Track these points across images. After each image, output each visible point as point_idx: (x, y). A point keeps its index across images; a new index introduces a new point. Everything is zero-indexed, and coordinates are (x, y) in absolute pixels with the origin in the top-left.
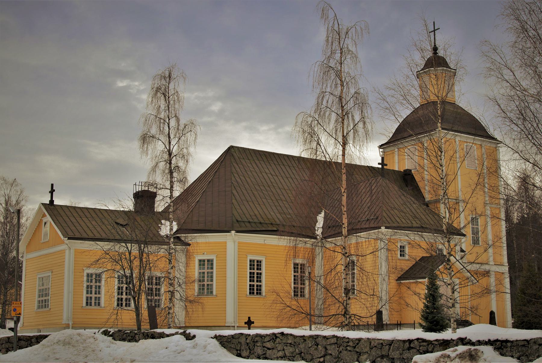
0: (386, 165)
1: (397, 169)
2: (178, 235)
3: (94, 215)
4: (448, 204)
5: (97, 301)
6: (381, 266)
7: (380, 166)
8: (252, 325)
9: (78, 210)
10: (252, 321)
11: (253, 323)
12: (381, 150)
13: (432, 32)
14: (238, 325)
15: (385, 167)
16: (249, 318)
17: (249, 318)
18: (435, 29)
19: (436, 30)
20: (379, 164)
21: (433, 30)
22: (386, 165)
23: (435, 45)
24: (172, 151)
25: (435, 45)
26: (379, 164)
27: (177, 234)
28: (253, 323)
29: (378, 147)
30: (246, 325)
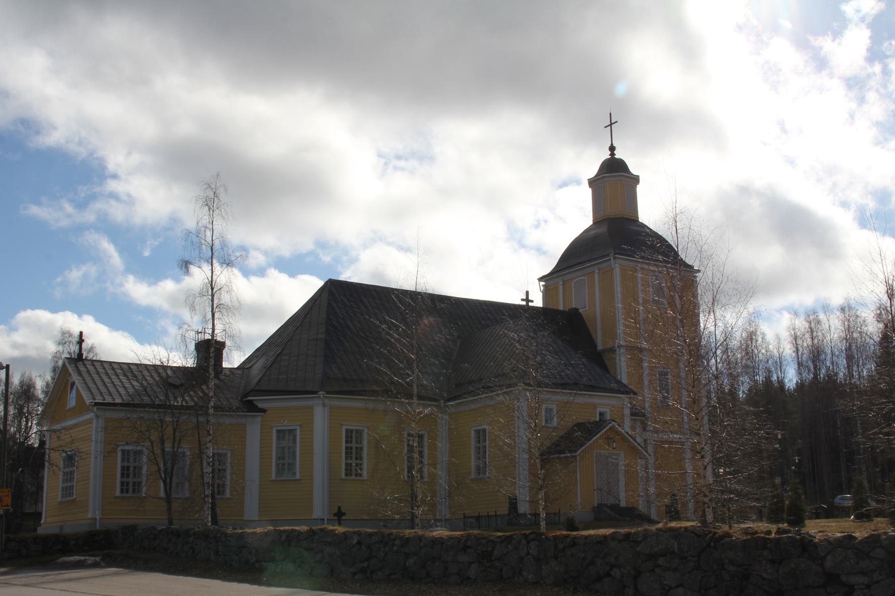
0: (532, 301)
1: (561, 308)
2: (250, 398)
3: (110, 372)
4: (719, 361)
5: (125, 487)
6: (86, 383)
7: (524, 303)
8: (343, 518)
9: (98, 365)
10: (343, 511)
11: (344, 514)
12: (542, 283)
13: (608, 126)
14: (329, 518)
15: (530, 304)
16: (339, 508)
17: (339, 508)
18: (612, 122)
19: (608, 126)
20: (522, 300)
21: (609, 124)
22: (532, 301)
23: (612, 144)
24: (802, 358)
25: (612, 144)
26: (522, 300)
27: (248, 397)
28: (344, 514)
29: (538, 279)
30: (336, 518)
